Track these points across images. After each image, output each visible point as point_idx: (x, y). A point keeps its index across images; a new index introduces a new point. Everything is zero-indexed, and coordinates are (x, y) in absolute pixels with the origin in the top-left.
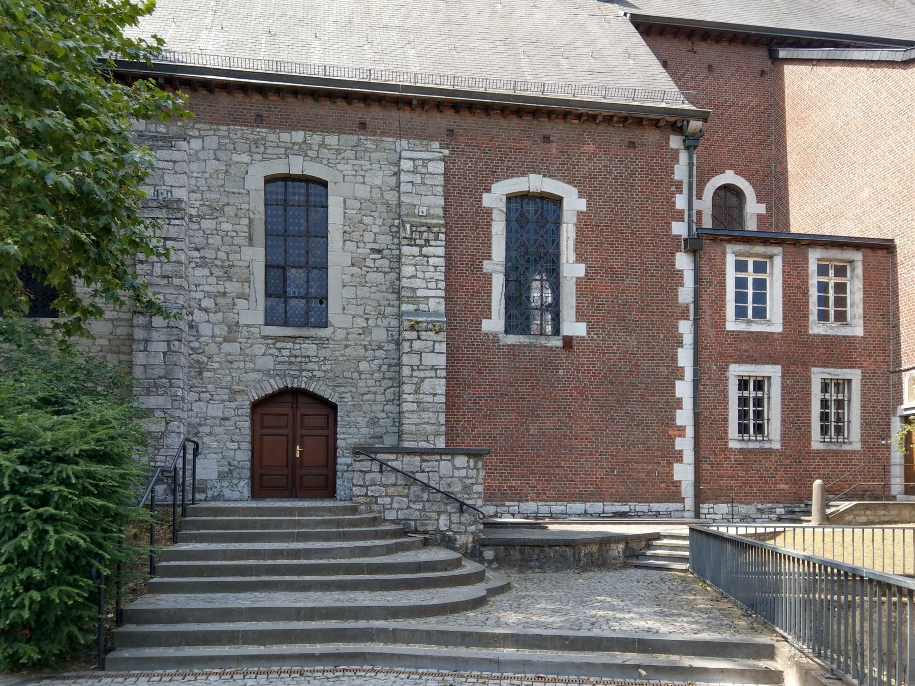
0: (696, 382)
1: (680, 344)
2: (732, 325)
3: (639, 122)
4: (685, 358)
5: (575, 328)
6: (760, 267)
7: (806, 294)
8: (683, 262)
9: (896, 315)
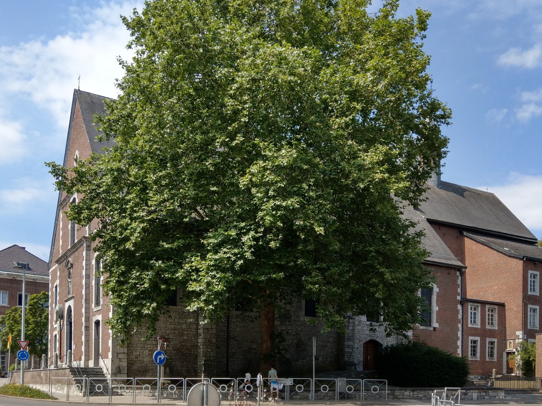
0: (462, 341)
1: (459, 330)
2: (469, 326)
3: (452, 268)
4: (460, 334)
5: (435, 325)
6: (475, 309)
7: (485, 317)
8: (459, 307)
9: (505, 324)
